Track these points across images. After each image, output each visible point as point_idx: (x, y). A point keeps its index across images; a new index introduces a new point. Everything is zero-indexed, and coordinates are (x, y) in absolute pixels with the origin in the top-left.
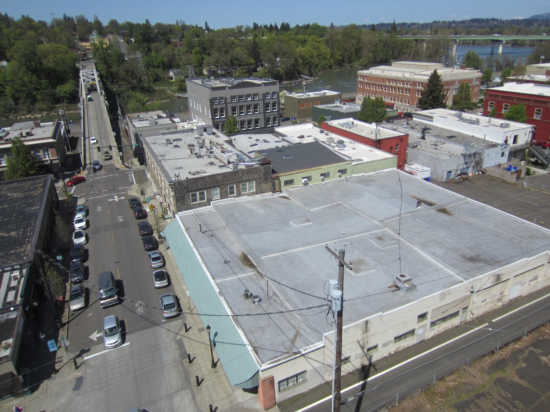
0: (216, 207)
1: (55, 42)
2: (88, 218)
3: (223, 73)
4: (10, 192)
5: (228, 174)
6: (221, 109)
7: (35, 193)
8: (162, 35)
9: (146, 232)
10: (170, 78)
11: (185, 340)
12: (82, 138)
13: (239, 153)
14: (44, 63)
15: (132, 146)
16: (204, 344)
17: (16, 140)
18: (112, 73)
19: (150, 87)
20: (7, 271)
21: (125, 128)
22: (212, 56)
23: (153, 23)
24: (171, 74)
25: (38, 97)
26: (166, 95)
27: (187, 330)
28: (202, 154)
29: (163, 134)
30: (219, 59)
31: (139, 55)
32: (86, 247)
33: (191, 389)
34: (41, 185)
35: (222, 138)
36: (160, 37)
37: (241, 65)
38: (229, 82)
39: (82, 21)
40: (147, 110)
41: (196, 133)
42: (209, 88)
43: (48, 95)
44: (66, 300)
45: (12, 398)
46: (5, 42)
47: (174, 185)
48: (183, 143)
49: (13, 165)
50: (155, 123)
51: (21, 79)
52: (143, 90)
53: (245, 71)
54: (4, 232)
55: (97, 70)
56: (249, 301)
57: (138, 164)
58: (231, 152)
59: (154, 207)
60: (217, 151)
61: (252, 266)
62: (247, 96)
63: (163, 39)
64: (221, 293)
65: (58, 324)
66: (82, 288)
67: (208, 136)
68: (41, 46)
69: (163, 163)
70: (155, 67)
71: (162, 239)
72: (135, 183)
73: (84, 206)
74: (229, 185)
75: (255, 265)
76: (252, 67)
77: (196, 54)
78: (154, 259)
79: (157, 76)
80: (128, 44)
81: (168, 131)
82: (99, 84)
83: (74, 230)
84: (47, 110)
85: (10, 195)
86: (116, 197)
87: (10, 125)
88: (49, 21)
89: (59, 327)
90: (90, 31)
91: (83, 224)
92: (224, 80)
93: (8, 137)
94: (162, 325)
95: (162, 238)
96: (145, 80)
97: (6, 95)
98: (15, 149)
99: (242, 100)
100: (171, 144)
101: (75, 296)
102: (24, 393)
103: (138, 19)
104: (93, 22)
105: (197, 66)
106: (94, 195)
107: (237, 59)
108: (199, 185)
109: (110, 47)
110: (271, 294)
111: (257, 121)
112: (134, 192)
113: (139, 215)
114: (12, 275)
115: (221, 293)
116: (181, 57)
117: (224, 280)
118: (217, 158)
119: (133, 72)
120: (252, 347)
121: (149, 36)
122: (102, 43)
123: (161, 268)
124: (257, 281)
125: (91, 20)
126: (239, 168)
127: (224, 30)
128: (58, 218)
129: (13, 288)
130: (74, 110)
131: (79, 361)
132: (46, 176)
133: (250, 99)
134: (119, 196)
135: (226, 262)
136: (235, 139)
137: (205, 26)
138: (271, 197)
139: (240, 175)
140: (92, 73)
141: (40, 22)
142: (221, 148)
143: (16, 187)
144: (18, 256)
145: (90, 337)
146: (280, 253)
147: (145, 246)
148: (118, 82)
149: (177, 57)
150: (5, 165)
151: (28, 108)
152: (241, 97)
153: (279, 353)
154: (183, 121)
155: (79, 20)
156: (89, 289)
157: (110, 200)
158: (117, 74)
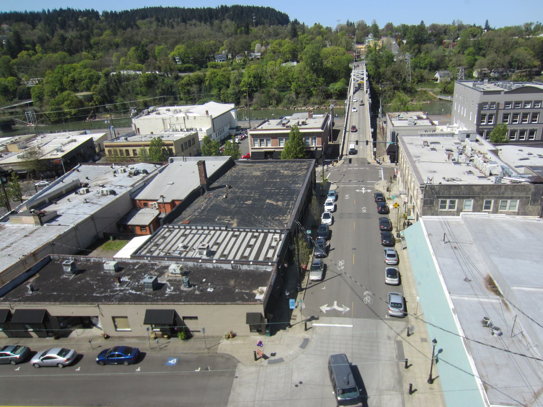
0: (465, 219)
1: (336, 45)
2: (336, 203)
3: (496, 76)
4: (283, 170)
5: (488, 187)
6: (489, 115)
7: (301, 173)
8: (435, 36)
9: (385, 228)
10: (434, 80)
11: (405, 344)
12: (344, 131)
13: (506, 166)
14: (324, 63)
15: (386, 143)
16: (424, 355)
17: (294, 127)
18: (379, 74)
19: (413, 88)
20: (271, 233)
21: (383, 126)
22: (487, 57)
23: (427, 24)
24: (437, 75)
25: (314, 92)
26: (427, 96)
27: (409, 335)
28: (460, 161)
29: (422, 135)
30: (495, 60)
31: (408, 55)
32: (331, 228)
33: (402, 394)
34: (306, 167)
35: (486, 146)
36: (433, 38)
37: (522, 67)
38: (506, 86)
39: (362, 26)
40: (408, 111)
41: (457, 138)
42: (481, 92)
43: (322, 91)
44: (307, 269)
45: (257, 333)
46: (298, 47)
47: (426, 188)
48: (441, 147)
49: (288, 147)
50: (414, 123)
51: (304, 77)
52: (405, 90)
53: (524, 74)
54: (274, 201)
55: (367, 71)
56: (487, 330)
57: (390, 161)
58: (495, 163)
59: (399, 205)
60: (478, 160)
61: (497, 292)
62: (526, 103)
63: (435, 41)
64: (455, 311)
65: (299, 288)
66: (322, 263)
67: (471, 143)
68: (324, 49)
69: (417, 164)
70: (421, 68)
71: (400, 238)
72: (383, 179)
73: (335, 192)
74: (485, 198)
75: (502, 293)
76: (535, 69)
77: (469, 55)
78: (390, 256)
79: (422, 77)
80: (399, 45)
81: (426, 133)
82: (367, 83)
83: (323, 211)
84: (318, 104)
85: (282, 171)
86: (363, 189)
87: (291, 115)
88: (334, 28)
89: (298, 290)
90: (366, 35)
91: (332, 207)
92: (500, 83)
93: (288, 124)
94: (385, 321)
95: (400, 237)
96: (409, 80)
97: (291, 90)
98: (292, 135)
99: (519, 106)
100: (428, 146)
101: (315, 268)
102: (265, 334)
103: (413, 21)
104: (370, 26)
105: (467, 68)
106: (344, 183)
107: (517, 60)
108: (452, 192)
109: (383, 48)
110: (516, 332)
111: (532, 133)
112: (381, 187)
113: (382, 210)
114: (274, 237)
115: (455, 311)
116: (451, 58)
117: (462, 298)
118: (476, 168)
119: (399, 73)
120: (482, 381)
121: (422, 37)
122: (375, 45)
123: (394, 266)
124: (501, 312)
125: (369, 24)
126: (502, 182)
127: (507, 29)
128: (314, 197)
129: (273, 247)
130: (340, 105)
131: (308, 324)
132: (311, 161)
133: (529, 106)
134: (367, 188)
135: (466, 280)
136: (501, 150)
137: (485, 25)
138: (536, 221)
139: (503, 190)
140: (362, 73)
141: (327, 28)
142: (484, 157)
143: (287, 166)
144: (281, 223)
145: (321, 308)
146: (537, 290)
147: (382, 241)
148: (383, 81)
149: (447, 58)
150: (283, 147)
151: (305, 101)
152: (517, 103)
153: (514, 402)
154: (441, 124)
155: (359, 25)
156: (327, 265)
157: (358, 191)
158: (384, 74)
